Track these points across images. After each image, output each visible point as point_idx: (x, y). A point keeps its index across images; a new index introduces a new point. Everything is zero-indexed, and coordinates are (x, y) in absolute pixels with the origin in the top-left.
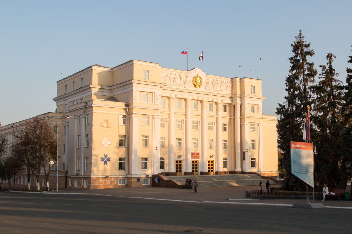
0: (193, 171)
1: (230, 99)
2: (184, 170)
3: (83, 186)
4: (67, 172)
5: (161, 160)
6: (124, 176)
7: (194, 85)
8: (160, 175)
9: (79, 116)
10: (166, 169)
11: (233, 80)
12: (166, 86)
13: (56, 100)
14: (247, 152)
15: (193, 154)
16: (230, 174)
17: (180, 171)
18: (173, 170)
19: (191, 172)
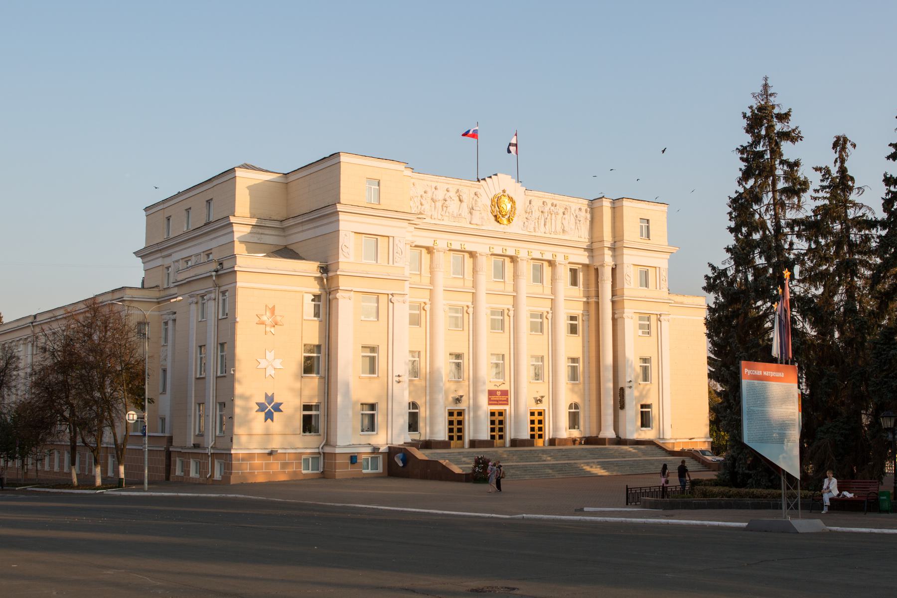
0: (493, 437)
1: (586, 254)
4: (170, 440)
5: (409, 409)
7: (496, 216)
8: (406, 447)
9: (202, 297)
10: (424, 433)
11: (594, 205)
14: (630, 387)
17: (458, 436)
18: (442, 434)
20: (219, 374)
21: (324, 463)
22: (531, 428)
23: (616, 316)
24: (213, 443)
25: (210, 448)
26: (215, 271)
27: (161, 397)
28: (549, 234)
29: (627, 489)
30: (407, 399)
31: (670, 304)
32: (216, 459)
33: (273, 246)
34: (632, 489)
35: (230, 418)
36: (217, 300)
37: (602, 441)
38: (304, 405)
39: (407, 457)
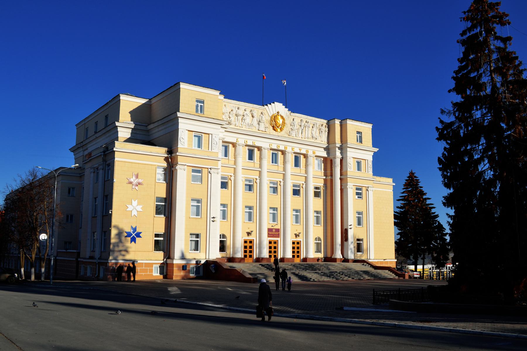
3: (97, 277)
5: (220, 238)
7: (273, 127)
10: (229, 252)
18: (240, 255)
20: (104, 214)
34: (391, 291)
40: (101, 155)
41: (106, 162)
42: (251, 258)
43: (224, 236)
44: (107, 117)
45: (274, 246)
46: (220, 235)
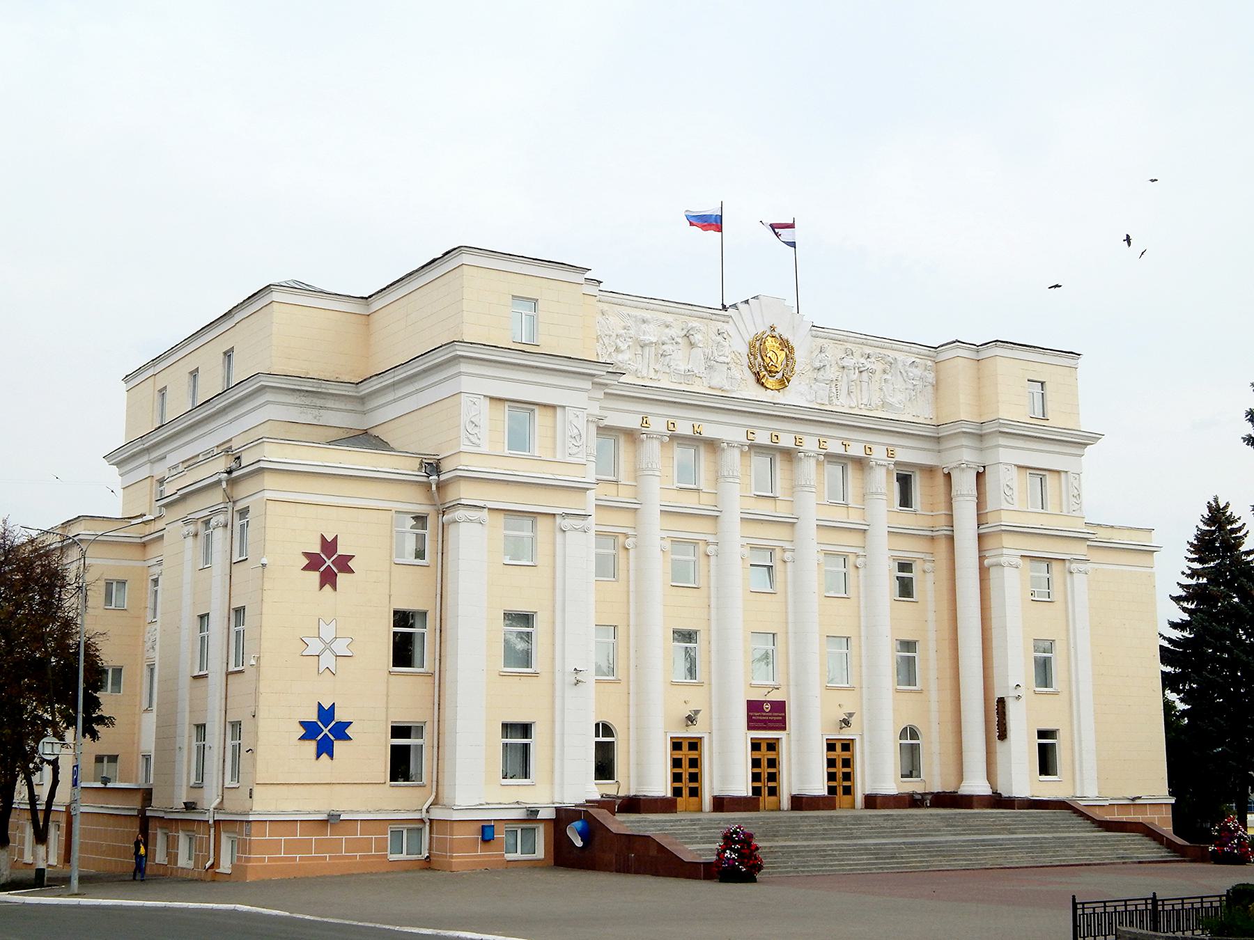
0: (756, 791)
2: (712, 788)
3: (212, 866)
4: (147, 795)
5: (597, 735)
6: (417, 816)
7: (757, 374)
8: (590, 810)
9: (207, 523)
10: (625, 784)
12: (623, 379)
13: (122, 458)
15: (753, 706)
16: (933, 805)
17: (691, 789)
18: (660, 786)
19: (745, 798)
20: (232, 668)
21: (431, 838)
22: (753, 774)
23: (986, 562)
24: (218, 800)
25: (212, 810)
26: (227, 472)
27: (145, 715)
28: (857, 408)
29: (1075, 904)
30: (594, 661)
31: (1089, 543)
32: (225, 832)
33: (342, 430)
34: (1086, 906)
35: (247, 751)
36: (229, 526)
37: (966, 802)
38: (392, 727)
39: (592, 829)
40: (219, 482)
41: (234, 502)
42: (848, 796)
43: (606, 729)
44: (228, 354)
45: (770, 757)
46: (597, 725)
